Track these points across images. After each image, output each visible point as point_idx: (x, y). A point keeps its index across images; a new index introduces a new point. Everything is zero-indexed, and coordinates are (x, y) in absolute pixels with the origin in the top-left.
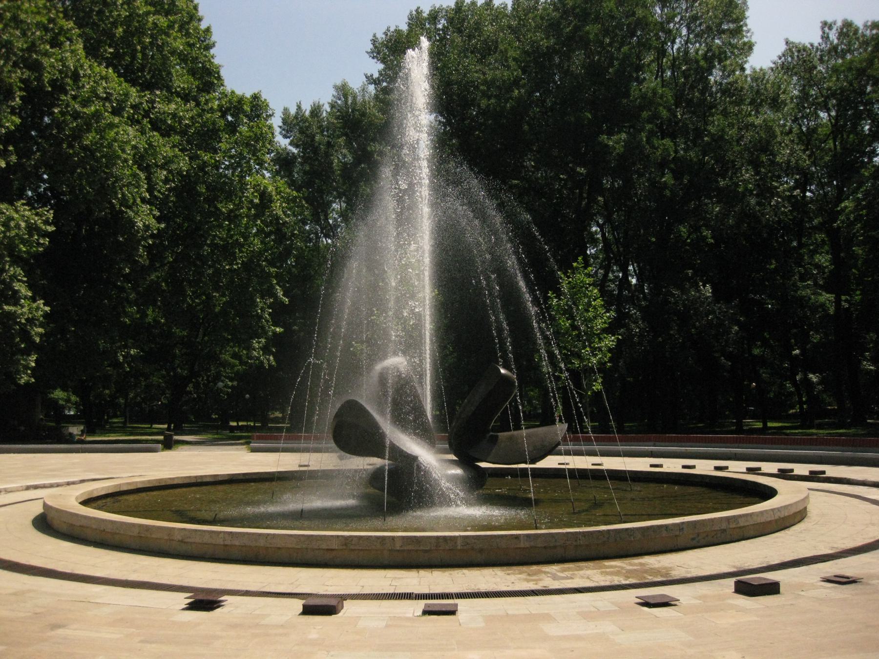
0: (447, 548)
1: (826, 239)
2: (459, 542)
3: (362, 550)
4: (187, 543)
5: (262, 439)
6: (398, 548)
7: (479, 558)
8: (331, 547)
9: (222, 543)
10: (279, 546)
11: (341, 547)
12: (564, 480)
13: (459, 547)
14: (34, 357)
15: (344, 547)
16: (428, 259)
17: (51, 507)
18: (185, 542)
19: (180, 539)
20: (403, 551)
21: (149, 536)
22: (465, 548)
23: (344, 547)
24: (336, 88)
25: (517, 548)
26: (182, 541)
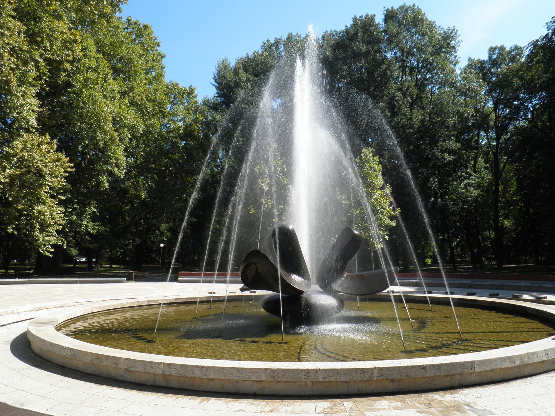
0: (365, 379)
1: (211, 136)
2: (375, 374)
3: (288, 382)
4: (131, 371)
5: (210, 276)
6: (321, 380)
7: (392, 387)
8: (261, 380)
9: (162, 373)
10: (212, 378)
11: (269, 380)
12: (449, 306)
13: (375, 378)
14: (184, 142)
15: (272, 379)
16: (253, 144)
17: (30, 331)
18: (129, 371)
19: (126, 368)
20: (324, 382)
21: (99, 363)
22: (380, 378)
23: (272, 379)
24: (353, 19)
25: (424, 377)
26: (127, 370)
